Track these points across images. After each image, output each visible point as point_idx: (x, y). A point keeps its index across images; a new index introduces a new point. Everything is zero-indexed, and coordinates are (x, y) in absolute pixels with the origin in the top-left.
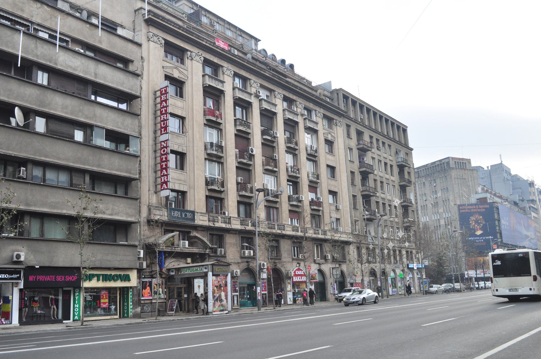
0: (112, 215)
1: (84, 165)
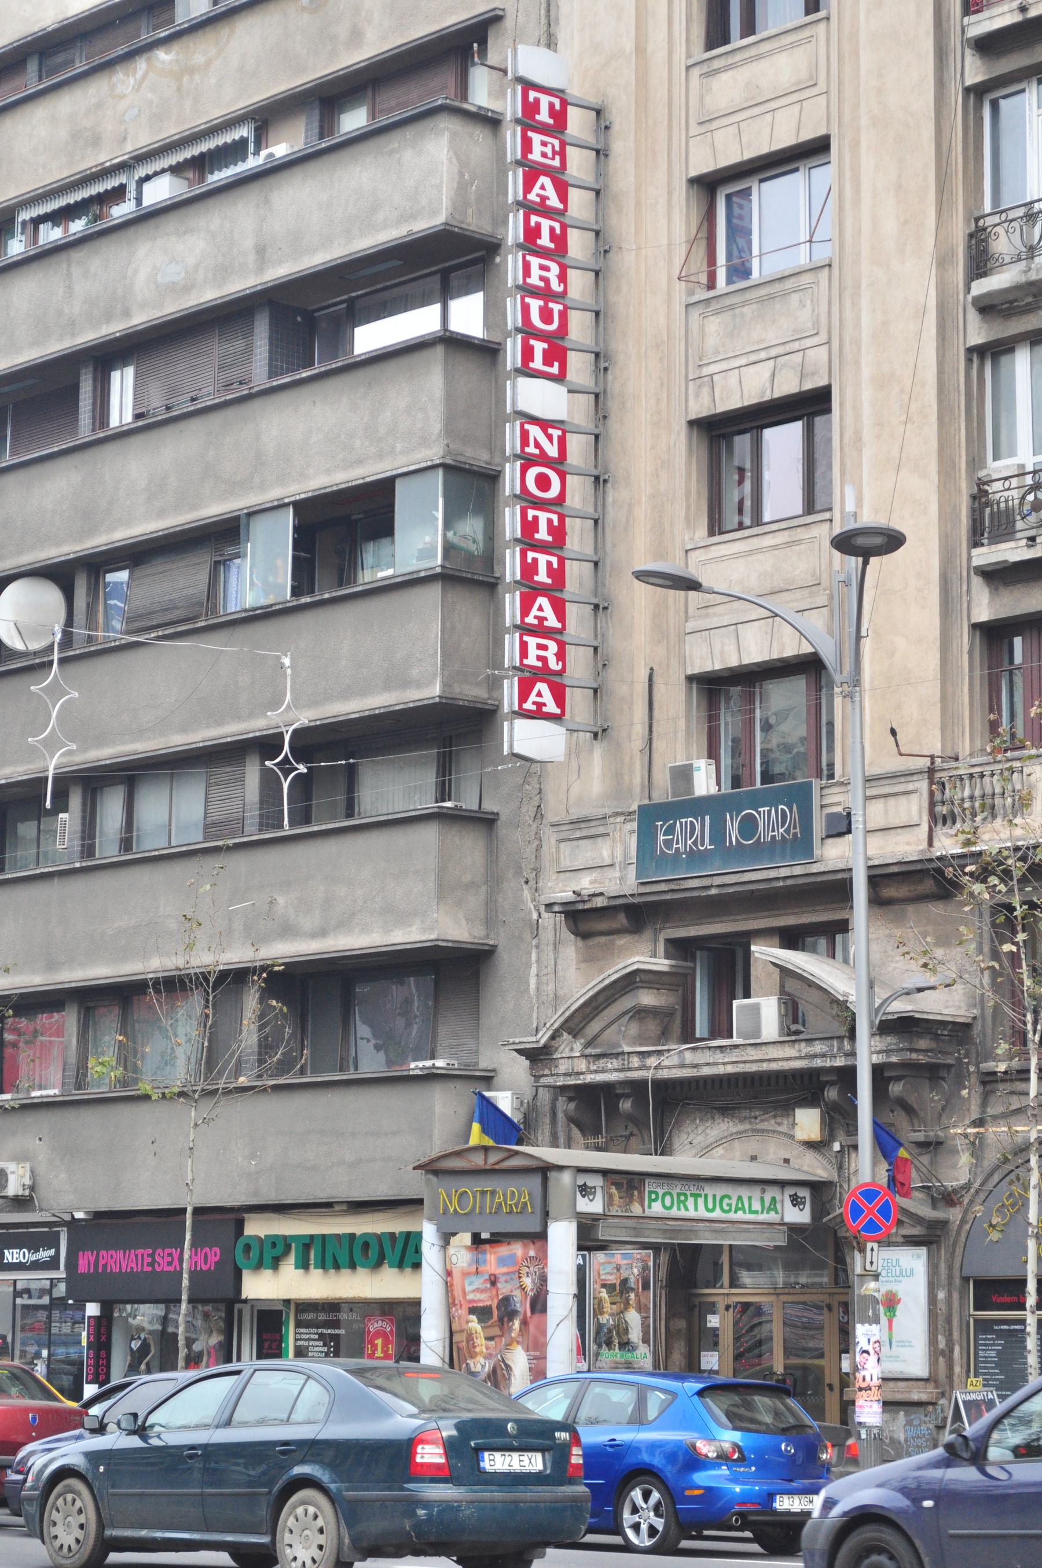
0: (322, 933)
1: (220, 723)
